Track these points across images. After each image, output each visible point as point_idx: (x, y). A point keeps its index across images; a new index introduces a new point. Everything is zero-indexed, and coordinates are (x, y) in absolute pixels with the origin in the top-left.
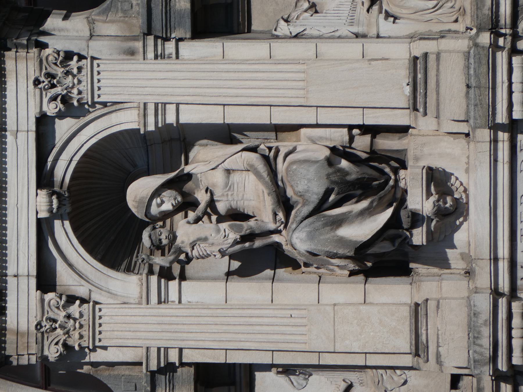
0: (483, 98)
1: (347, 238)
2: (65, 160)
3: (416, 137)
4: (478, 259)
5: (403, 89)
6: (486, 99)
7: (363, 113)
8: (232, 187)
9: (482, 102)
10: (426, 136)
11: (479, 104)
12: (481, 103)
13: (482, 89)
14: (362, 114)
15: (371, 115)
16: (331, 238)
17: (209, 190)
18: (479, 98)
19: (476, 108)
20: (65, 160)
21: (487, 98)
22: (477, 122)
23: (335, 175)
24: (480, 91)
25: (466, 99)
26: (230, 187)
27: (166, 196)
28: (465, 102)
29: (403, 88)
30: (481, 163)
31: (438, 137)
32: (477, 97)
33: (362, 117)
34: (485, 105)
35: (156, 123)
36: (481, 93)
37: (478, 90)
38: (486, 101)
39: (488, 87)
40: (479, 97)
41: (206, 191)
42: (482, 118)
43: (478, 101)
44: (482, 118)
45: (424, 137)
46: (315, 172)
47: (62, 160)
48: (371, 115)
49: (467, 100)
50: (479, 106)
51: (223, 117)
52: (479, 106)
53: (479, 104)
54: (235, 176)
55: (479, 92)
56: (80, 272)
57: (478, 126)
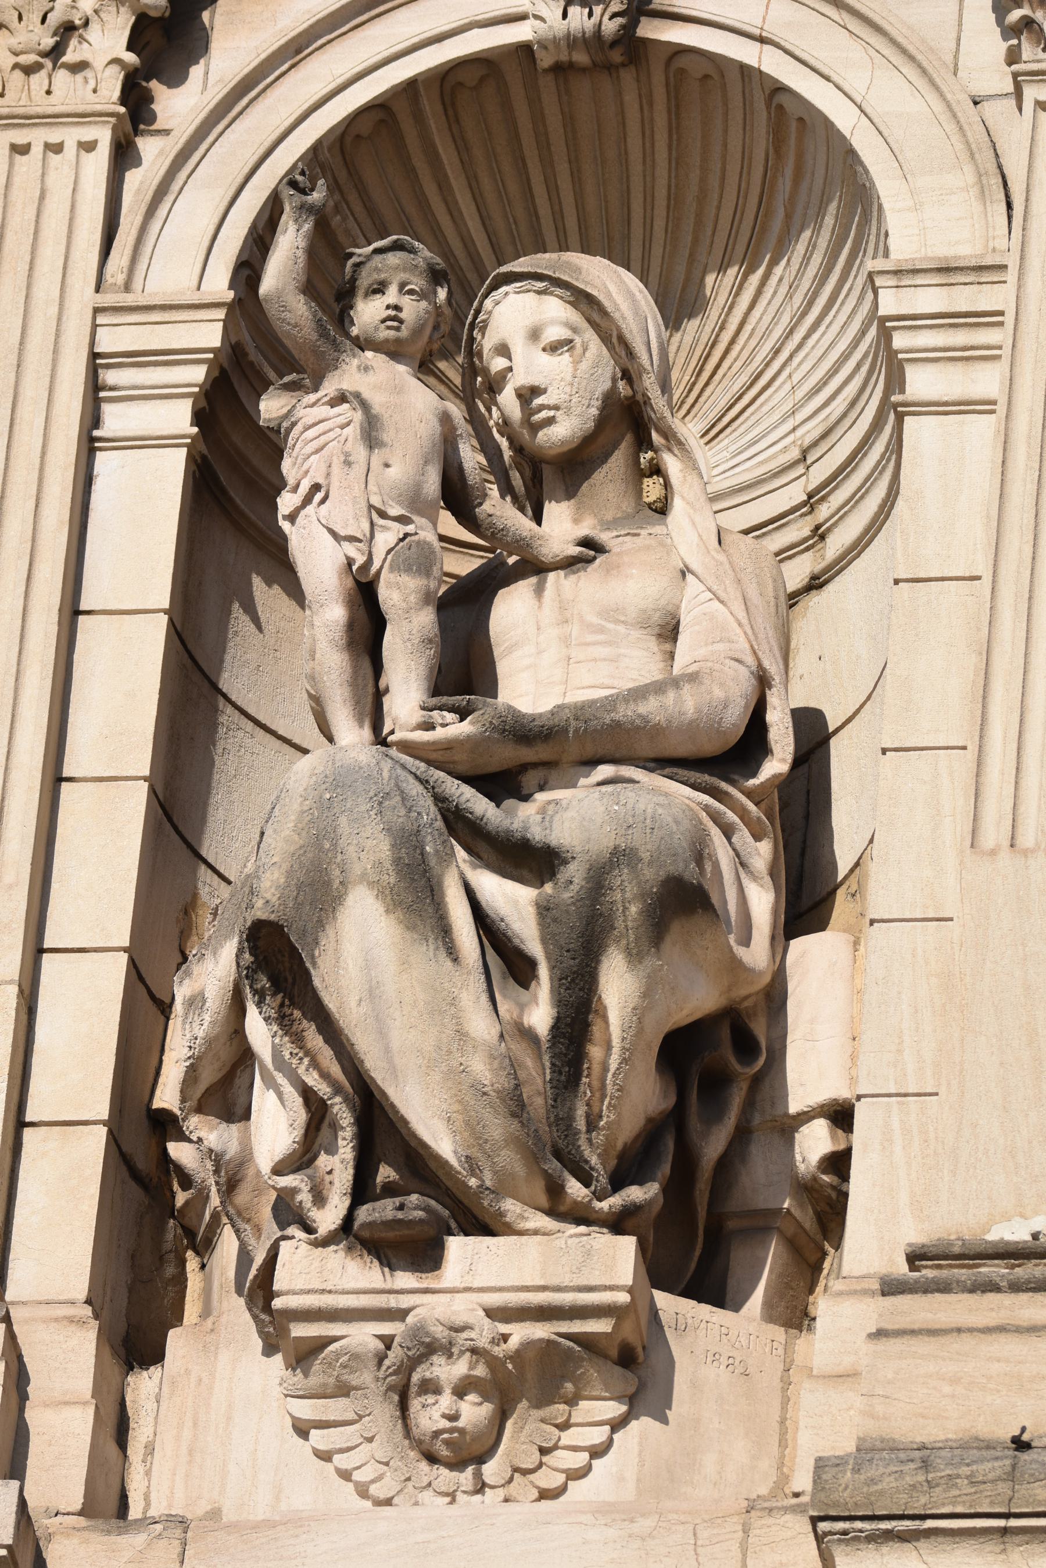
0: (957, 1492)
1: (335, 918)
2: (764, 19)
3: (781, 1351)
4: (184, 1544)
5: (1018, 1219)
6: (954, 1504)
7: (906, 1095)
8: (601, 637)
9: (937, 1490)
10: (784, 1390)
11: (930, 1476)
12: (938, 1485)
13: (1003, 1488)
14: (902, 1091)
15: (896, 1124)
16: (339, 857)
17: (592, 553)
18: (958, 1476)
19: (912, 1466)
20: (764, 19)
21: (959, 1509)
22: (844, 1472)
23: (628, 895)
24: (992, 1481)
25: (955, 1441)
26: (601, 630)
27: (576, 370)
28: (943, 1438)
29: (1022, 1216)
30: (643, 1539)
31: (776, 1438)
32: (966, 1469)
33: (893, 1091)
34: (923, 1500)
35: (912, 320)
36: (985, 1483)
37: (999, 1472)
38: (943, 1504)
39: (1014, 1510)
40: (967, 1477)
41: (587, 543)
42: (865, 1489)
43: (948, 1472)
44: (865, 1489)
45: (777, 1383)
46: (649, 816)
47: (760, 62)
48: (896, 1124)
49: (954, 1445)
50: (921, 1478)
51: (923, 575)
52: (921, 1478)
53: (930, 1476)
54: (645, 654)
55: (991, 1476)
56: (264, 90)
57: (824, 1477)
